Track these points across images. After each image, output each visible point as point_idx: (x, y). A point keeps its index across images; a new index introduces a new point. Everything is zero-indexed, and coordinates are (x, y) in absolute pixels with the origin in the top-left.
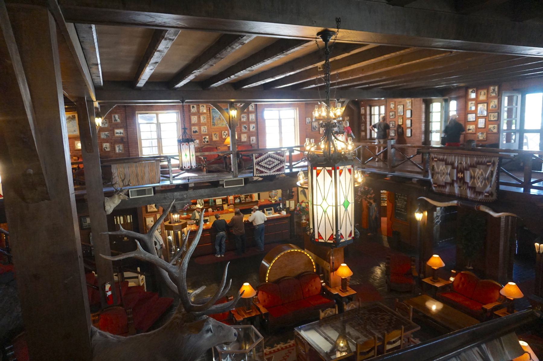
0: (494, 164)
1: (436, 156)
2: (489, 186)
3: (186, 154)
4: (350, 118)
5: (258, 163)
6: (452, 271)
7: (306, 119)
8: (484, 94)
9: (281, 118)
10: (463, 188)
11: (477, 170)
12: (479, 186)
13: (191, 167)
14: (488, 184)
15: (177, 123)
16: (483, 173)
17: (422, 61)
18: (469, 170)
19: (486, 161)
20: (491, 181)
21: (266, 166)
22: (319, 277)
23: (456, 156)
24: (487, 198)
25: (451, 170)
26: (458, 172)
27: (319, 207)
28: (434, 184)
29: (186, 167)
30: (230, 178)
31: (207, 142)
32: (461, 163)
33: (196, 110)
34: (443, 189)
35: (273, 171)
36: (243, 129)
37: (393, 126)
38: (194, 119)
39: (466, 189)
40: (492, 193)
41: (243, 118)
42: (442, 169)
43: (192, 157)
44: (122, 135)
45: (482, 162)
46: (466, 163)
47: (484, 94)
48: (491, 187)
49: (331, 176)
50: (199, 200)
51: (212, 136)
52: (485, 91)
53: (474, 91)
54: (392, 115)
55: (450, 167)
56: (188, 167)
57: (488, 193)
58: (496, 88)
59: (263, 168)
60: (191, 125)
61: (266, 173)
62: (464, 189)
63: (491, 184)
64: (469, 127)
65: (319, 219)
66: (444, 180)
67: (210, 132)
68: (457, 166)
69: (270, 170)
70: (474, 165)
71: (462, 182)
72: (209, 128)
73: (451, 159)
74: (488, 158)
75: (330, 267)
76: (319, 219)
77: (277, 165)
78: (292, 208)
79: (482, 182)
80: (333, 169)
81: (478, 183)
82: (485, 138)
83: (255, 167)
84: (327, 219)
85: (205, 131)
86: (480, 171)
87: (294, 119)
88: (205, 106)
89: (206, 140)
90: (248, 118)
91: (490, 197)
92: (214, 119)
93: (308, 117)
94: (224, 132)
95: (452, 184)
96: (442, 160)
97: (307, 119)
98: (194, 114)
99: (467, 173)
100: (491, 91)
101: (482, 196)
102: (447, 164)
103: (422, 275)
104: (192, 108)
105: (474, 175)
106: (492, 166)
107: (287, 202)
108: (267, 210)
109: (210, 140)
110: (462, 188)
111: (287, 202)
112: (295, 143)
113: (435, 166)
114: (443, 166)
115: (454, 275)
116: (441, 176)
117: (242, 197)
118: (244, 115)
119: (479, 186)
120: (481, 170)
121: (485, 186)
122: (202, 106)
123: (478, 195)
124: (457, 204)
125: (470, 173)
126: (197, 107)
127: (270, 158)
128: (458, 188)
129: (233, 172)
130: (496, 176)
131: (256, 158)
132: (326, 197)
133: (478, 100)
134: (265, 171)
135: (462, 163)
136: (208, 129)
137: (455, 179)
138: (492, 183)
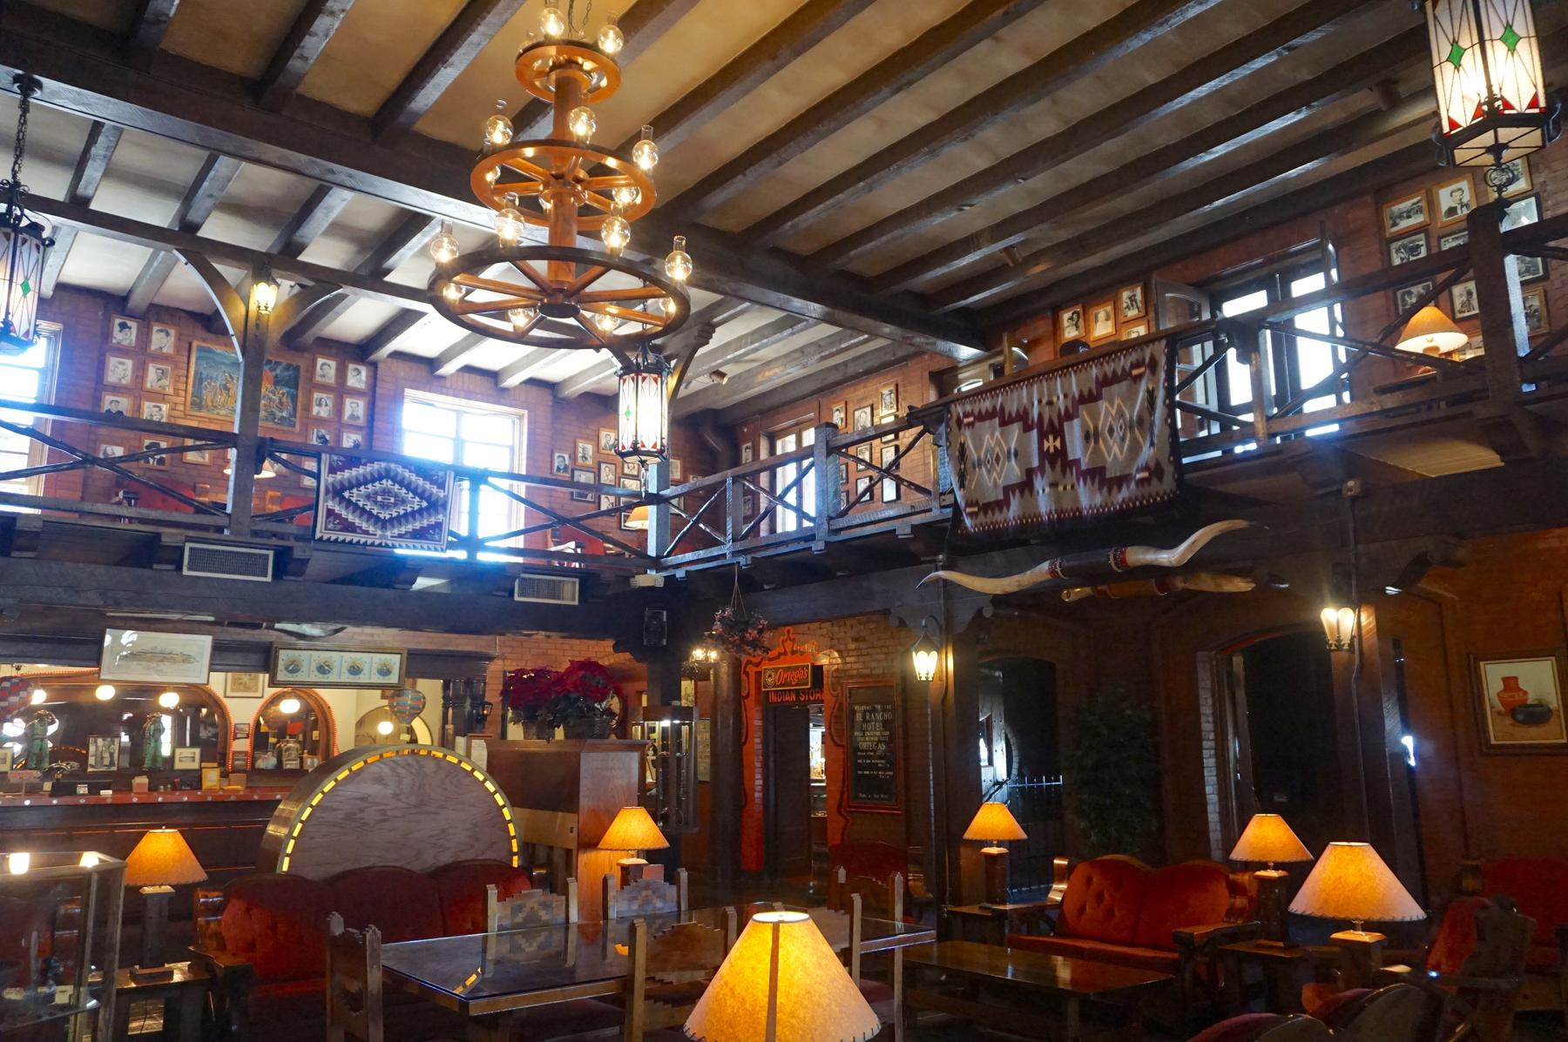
0: (1153, 365)
1: (968, 408)
2: (1148, 443)
5: (337, 492)
6: (1056, 862)
7: (552, 456)
8: (1107, 319)
9: (464, 436)
10: (1065, 488)
11: (1103, 405)
14: (1140, 439)
15: (43, 372)
16: (1124, 408)
18: (1078, 417)
19: (1127, 368)
20: (1152, 424)
21: (368, 508)
22: (530, 877)
23: (1032, 385)
24: (1147, 490)
25: (1019, 440)
26: (1042, 437)
28: (968, 504)
32: (1050, 403)
34: (998, 517)
35: (396, 531)
38: (119, 370)
39: (1073, 487)
40: (1158, 464)
41: (320, 405)
45: (1114, 372)
46: (1065, 396)
47: (1107, 319)
48: (1152, 444)
50: (100, 741)
52: (1109, 308)
53: (1078, 313)
55: (1016, 429)
57: (1146, 468)
58: (1139, 291)
59: (358, 512)
60: (100, 386)
61: (366, 532)
62: (1069, 487)
63: (1152, 434)
68: (1040, 416)
69: (384, 527)
70: (1090, 391)
72: (176, 413)
74: (1134, 354)
75: (575, 830)
77: (413, 513)
81: (1109, 450)
83: (325, 501)
86: (1112, 406)
87: (512, 449)
88: (172, 332)
90: (339, 409)
91: (1155, 481)
92: (201, 383)
93: (560, 450)
96: (989, 415)
97: (556, 455)
98: (122, 351)
99: (1072, 428)
100: (1125, 305)
101: (1128, 487)
104: (116, 329)
105: (1096, 429)
110: (1061, 488)
112: (510, 526)
113: (970, 445)
114: (992, 435)
115: (1064, 874)
117: (288, 749)
118: (324, 396)
120: (1117, 401)
121: (1135, 449)
122: (161, 331)
124: (1052, 572)
125: (1084, 424)
126: (138, 329)
127: (390, 482)
128: (1047, 490)
129: (229, 515)
130: (1164, 402)
131: (332, 470)
134: (364, 526)
135: (1055, 399)
137: (1035, 463)
138: (1156, 431)
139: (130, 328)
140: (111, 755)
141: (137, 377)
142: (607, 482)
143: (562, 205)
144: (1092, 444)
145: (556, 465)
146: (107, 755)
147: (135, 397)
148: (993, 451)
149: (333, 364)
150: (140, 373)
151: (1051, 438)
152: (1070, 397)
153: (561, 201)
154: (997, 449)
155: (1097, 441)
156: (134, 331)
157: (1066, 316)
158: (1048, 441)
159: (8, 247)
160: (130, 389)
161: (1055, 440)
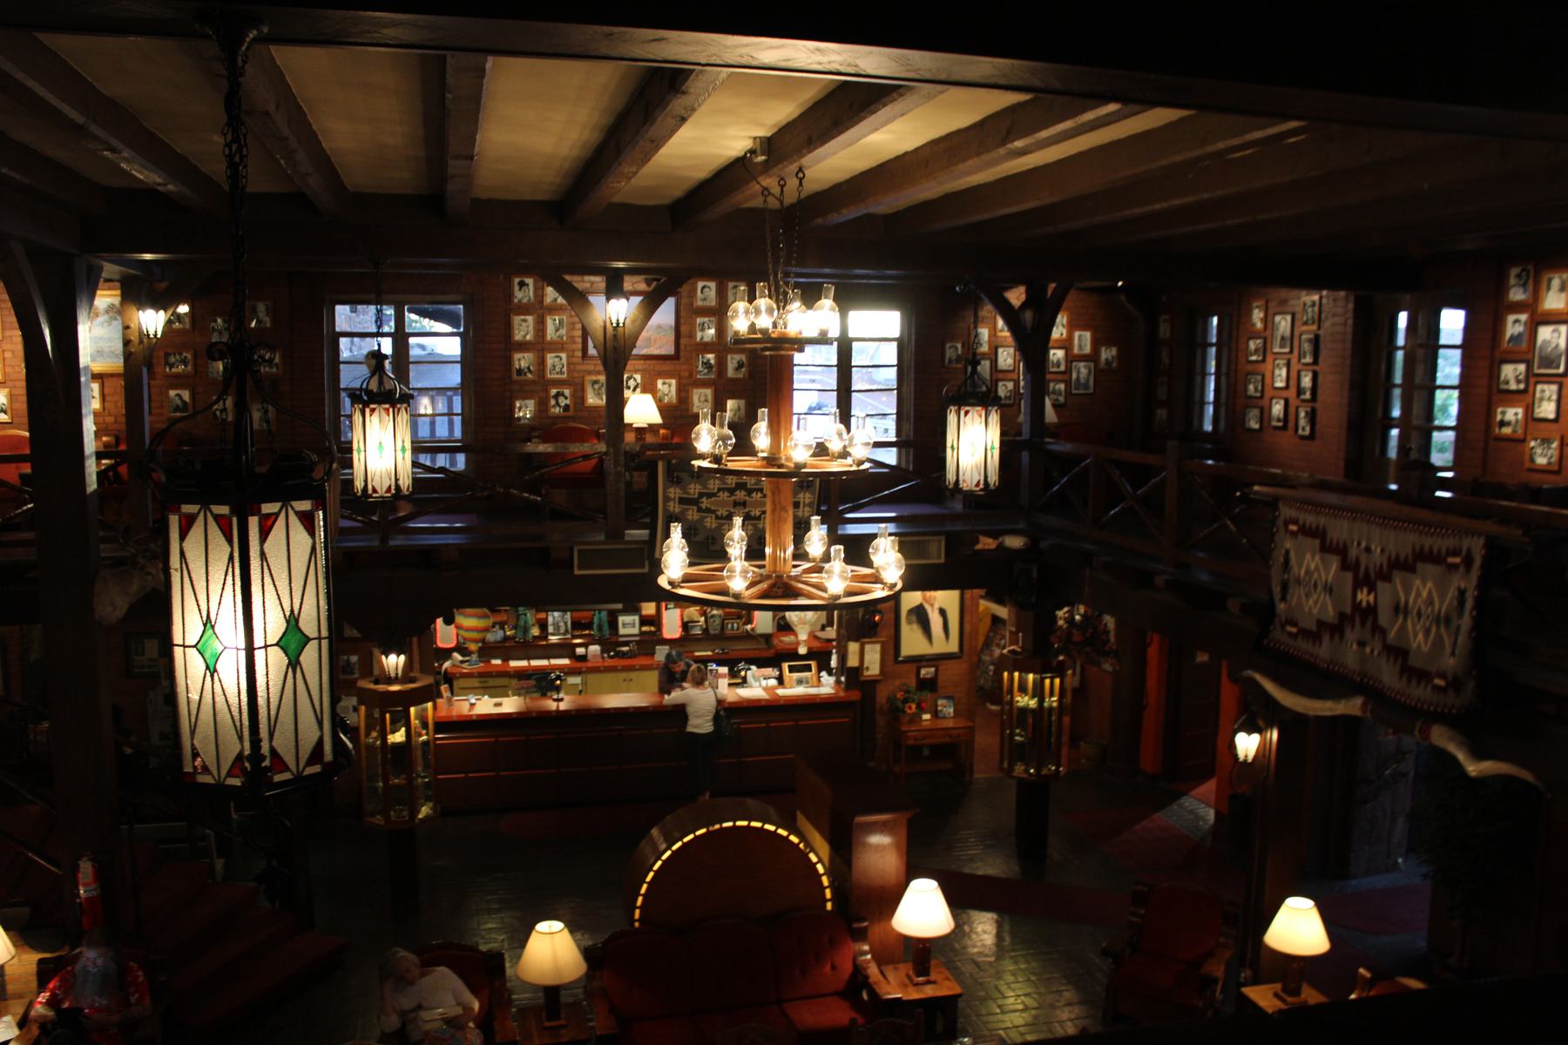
3: (380, 443)
4: (1119, 351)
10: (1372, 651)
12: (1419, 645)
13: (398, 487)
17: (1234, 136)
19: (1444, 551)
27: (192, 653)
29: (378, 489)
30: (600, 543)
31: (566, 408)
32: (1368, 550)
33: (531, 294)
36: (700, 368)
37: (1256, 390)
42: (1313, 566)
43: (400, 455)
44: (274, 370)
46: (1383, 551)
49: (230, 541)
51: (583, 390)
54: (1256, 351)
56: (384, 489)
64: (1503, 413)
65: (195, 696)
66: (1315, 611)
67: (576, 375)
71: (1369, 624)
72: (574, 360)
73: (1339, 530)
76: (195, 696)
78: (869, 673)
79: (1427, 631)
80: (233, 512)
81: (1416, 635)
82: (1553, 460)
84: (220, 699)
85: (558, 369)
86: (1424, 586)
89: (563, 402)
94: (629, 378)
95: (1336, 629)
102: (1325, 549)
103: (1245, 974)
104: (516, 288)
106: (1462, 569)
107: (853, 647)
108: (792, 669)
109: (575, 404)
110: (1368, 650)
111: (853, 647)
116: (1308, 595)
117: (713, 616)
118: (706, 319)
119: (1419, 645)
123: (1414, 683)
130: (1471, 612)
132: (213, 617)
133: (1540, 310)
135: (1373, 547)
136: (569, 364)
139: (528, 285)
140: (566, 623)
141: (538, 330)
142: (1005, 368)
143: (779, 492)
144: (1400, 620)
145: (948, 356)
146: (562, 624)
147: (538, 350)
148: (1311, 576)
149: (713, 285)
150: (541, 327)
151: (1365, 590)
152: (1387, 554)
153: (778, 488)
154: (1316, 575)
155: (1405, 619)
156: (531, 287)
157: (1514, 271)
158: (1362, 592)
159: (372, 480)
160: (534, 344)
161: (1369, 594)
